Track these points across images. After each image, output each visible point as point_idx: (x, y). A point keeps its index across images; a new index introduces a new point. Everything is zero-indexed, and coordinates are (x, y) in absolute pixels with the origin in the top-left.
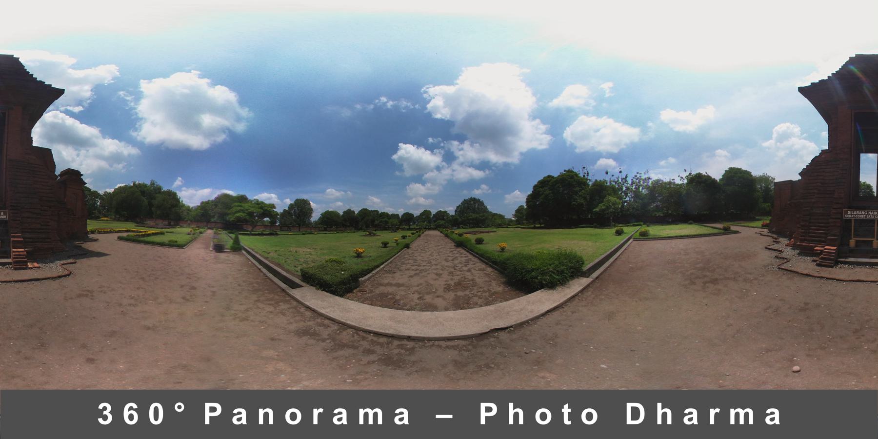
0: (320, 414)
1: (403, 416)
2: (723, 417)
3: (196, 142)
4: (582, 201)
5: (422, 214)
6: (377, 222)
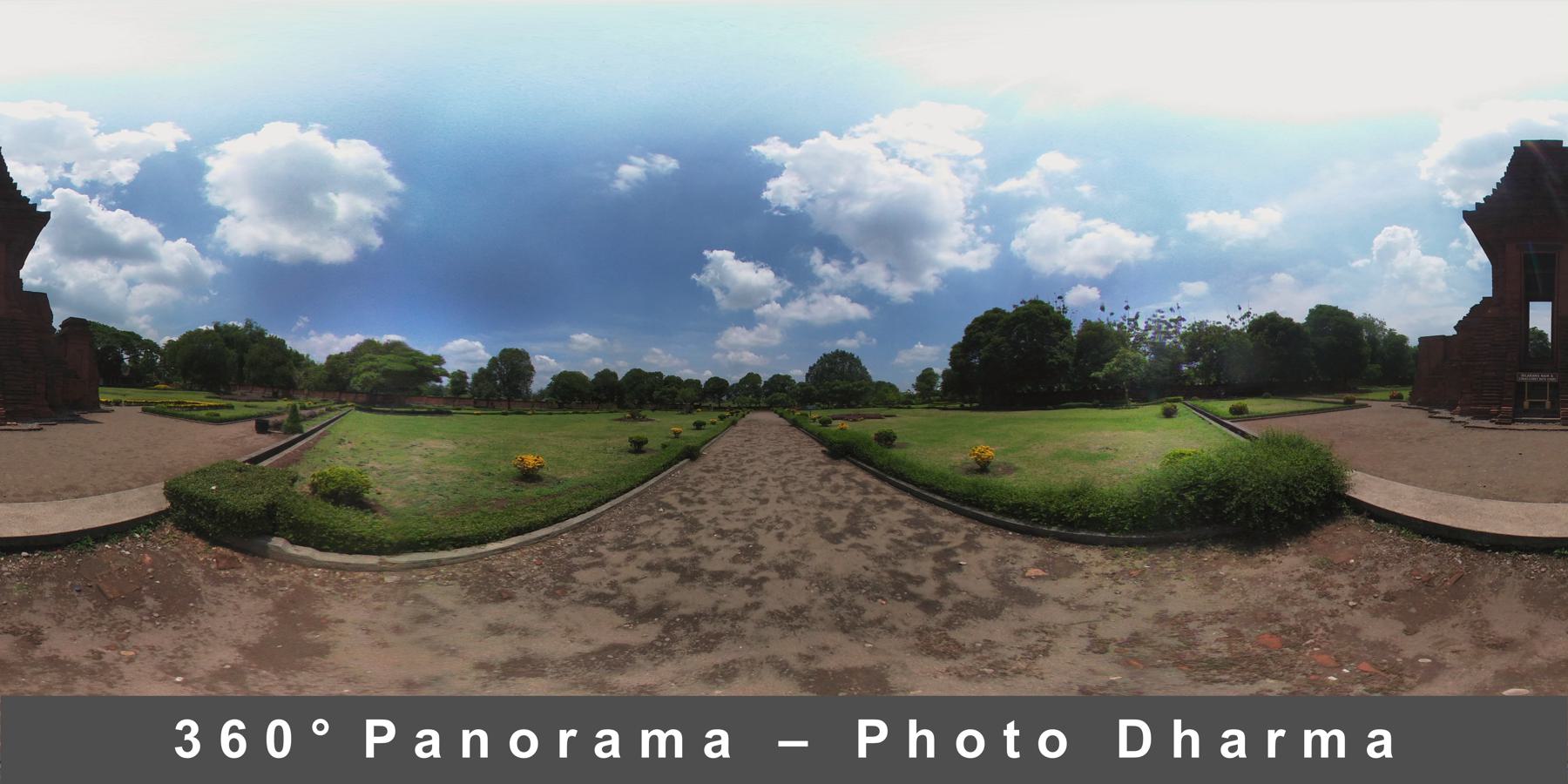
0: (571, 739)
1: (719, 744)
2: (1291, 745)
3: (336, 251)
4: (1067, 358)
5: (743, 381)
6: (656, 394)
